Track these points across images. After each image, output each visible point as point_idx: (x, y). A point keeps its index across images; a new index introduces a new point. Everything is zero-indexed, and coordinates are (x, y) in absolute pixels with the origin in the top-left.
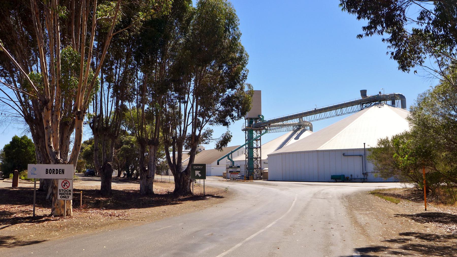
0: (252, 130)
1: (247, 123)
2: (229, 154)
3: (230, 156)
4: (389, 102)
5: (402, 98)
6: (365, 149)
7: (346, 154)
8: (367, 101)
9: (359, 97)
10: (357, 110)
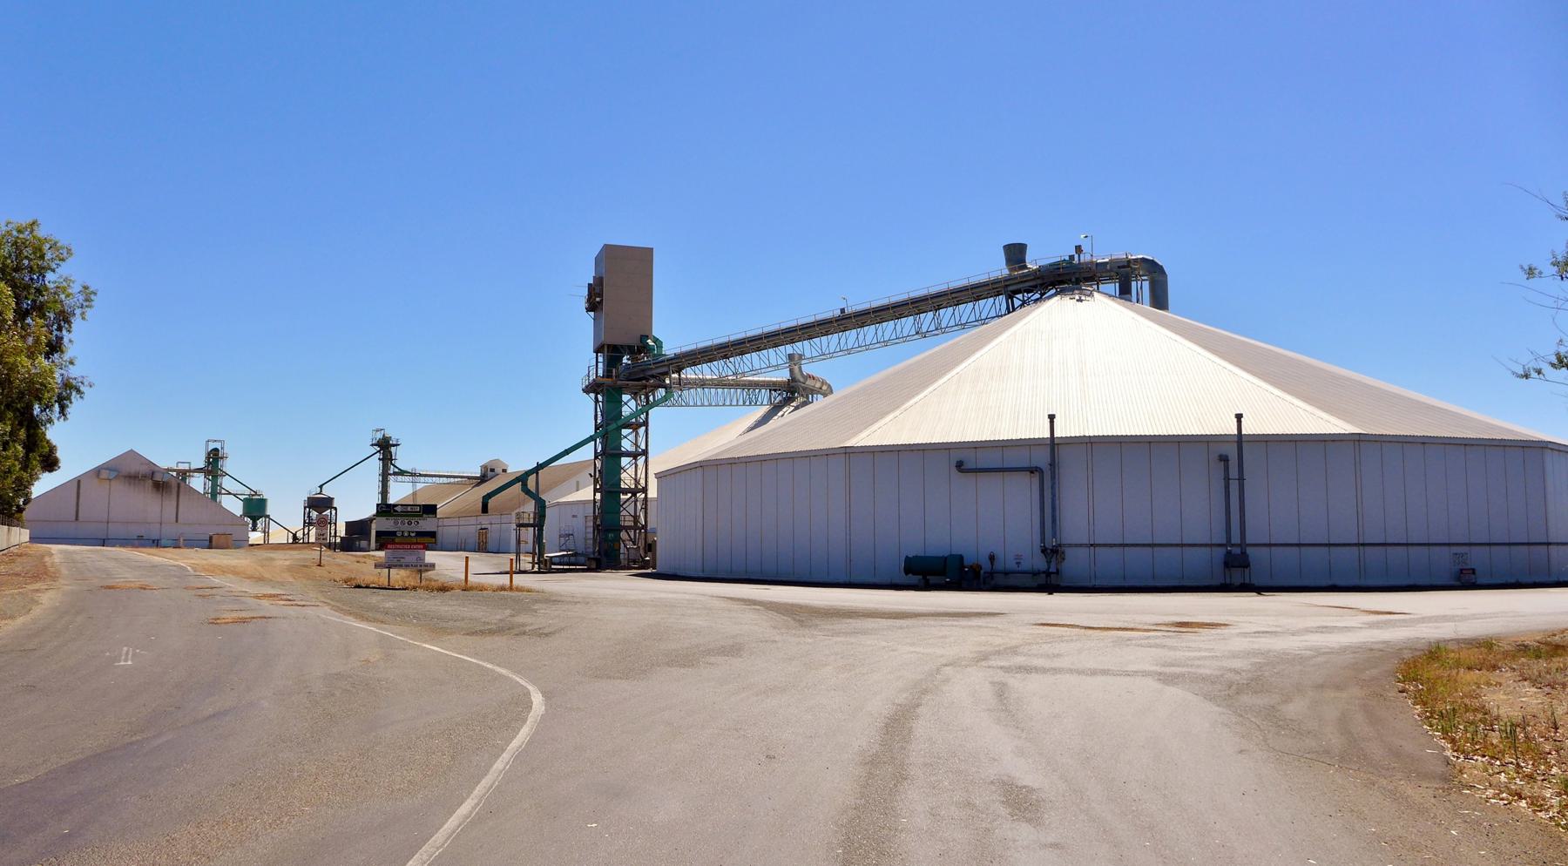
0: (620, 391)
1: (600, 365)
2: (528, 473)
3: (531, 480)
4: (1113, 287)
5: (1154, 270)
6: (1053, 444)
7: (970, 462)
8: (1028, 282)
9: (998, 268)
10: (993, 314)
